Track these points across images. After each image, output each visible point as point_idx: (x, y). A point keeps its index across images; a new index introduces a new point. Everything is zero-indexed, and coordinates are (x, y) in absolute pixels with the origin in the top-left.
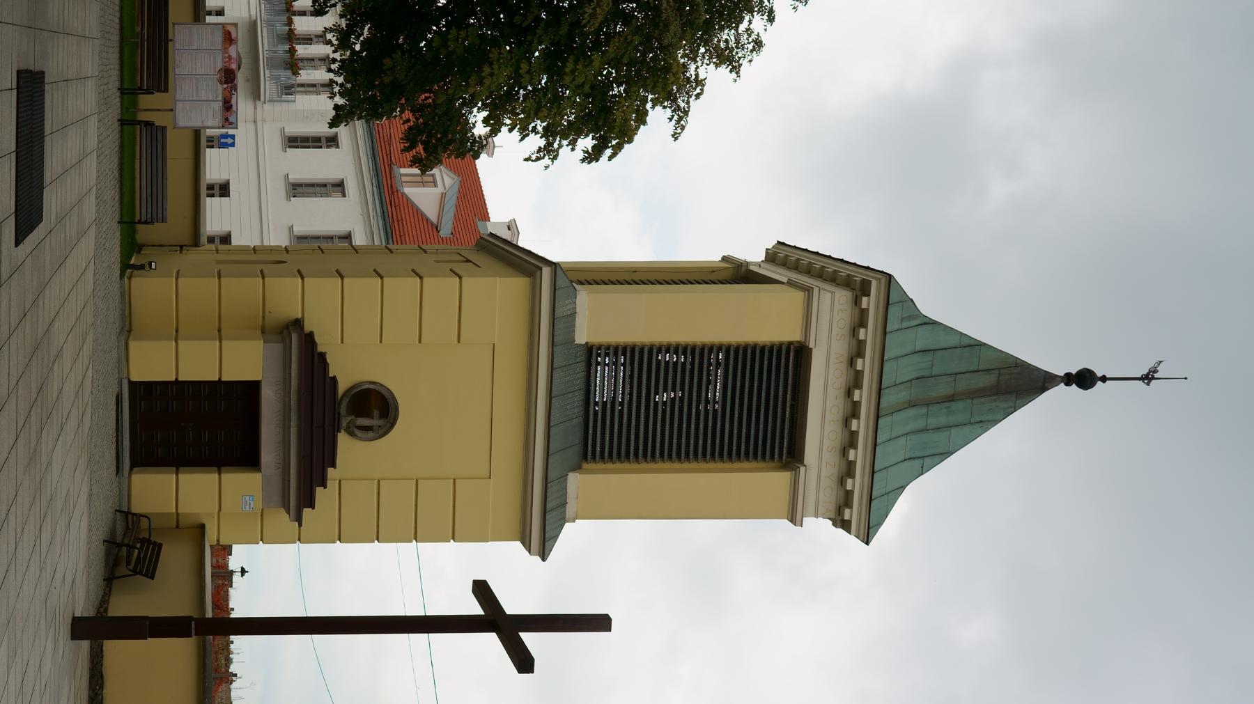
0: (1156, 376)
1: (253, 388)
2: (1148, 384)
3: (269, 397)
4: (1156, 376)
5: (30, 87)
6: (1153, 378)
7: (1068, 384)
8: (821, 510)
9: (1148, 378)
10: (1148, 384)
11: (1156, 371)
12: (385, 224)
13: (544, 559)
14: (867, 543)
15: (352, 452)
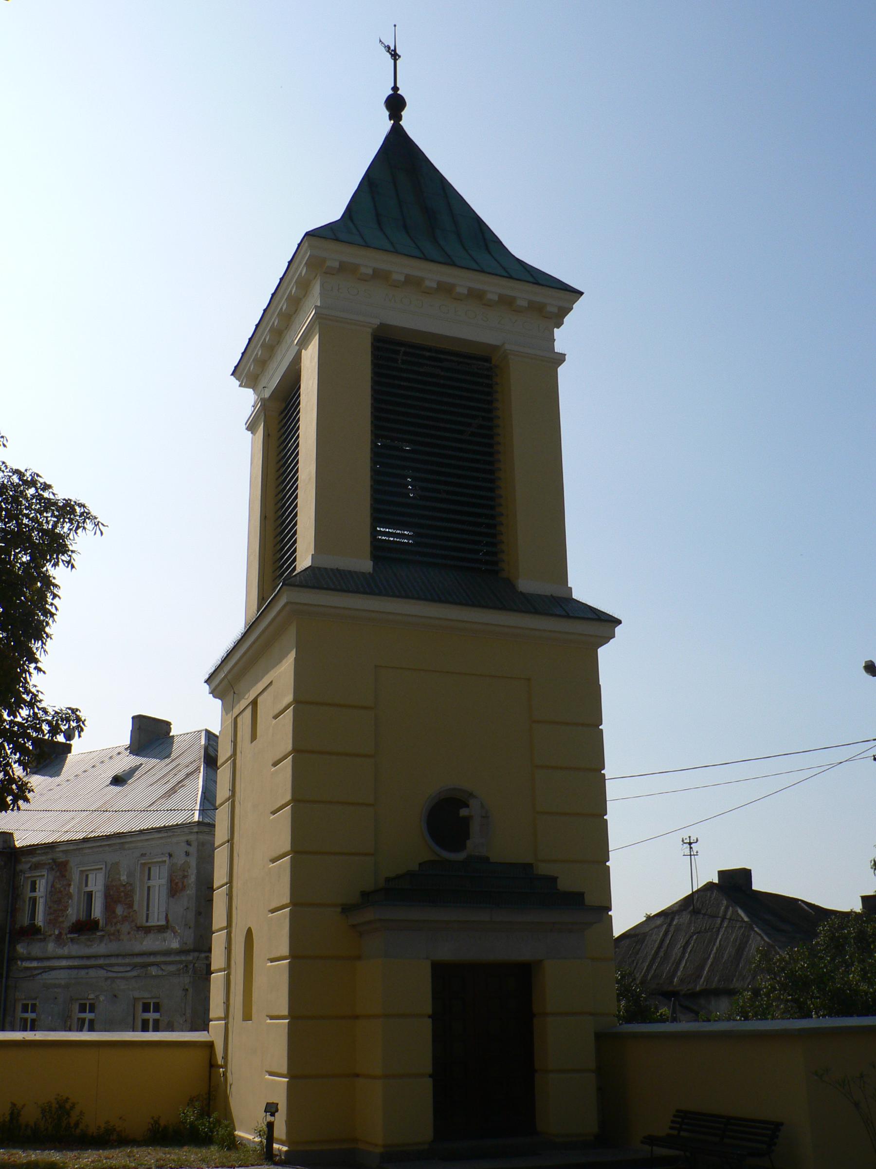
0: (392, 48)
1: (445, 976)
2: (399, 57)
3: (448, 951)
4: (392, 48)
5: (254, 737)
6: (395, 50)
7: (400, 118)
8: (157, 888)
9: (395, 56)
10: (399, 57)
11: (389, 47)
12: (14, 1011)
13: (619, 622)
14: (581, 293)
15: (502, 839)
